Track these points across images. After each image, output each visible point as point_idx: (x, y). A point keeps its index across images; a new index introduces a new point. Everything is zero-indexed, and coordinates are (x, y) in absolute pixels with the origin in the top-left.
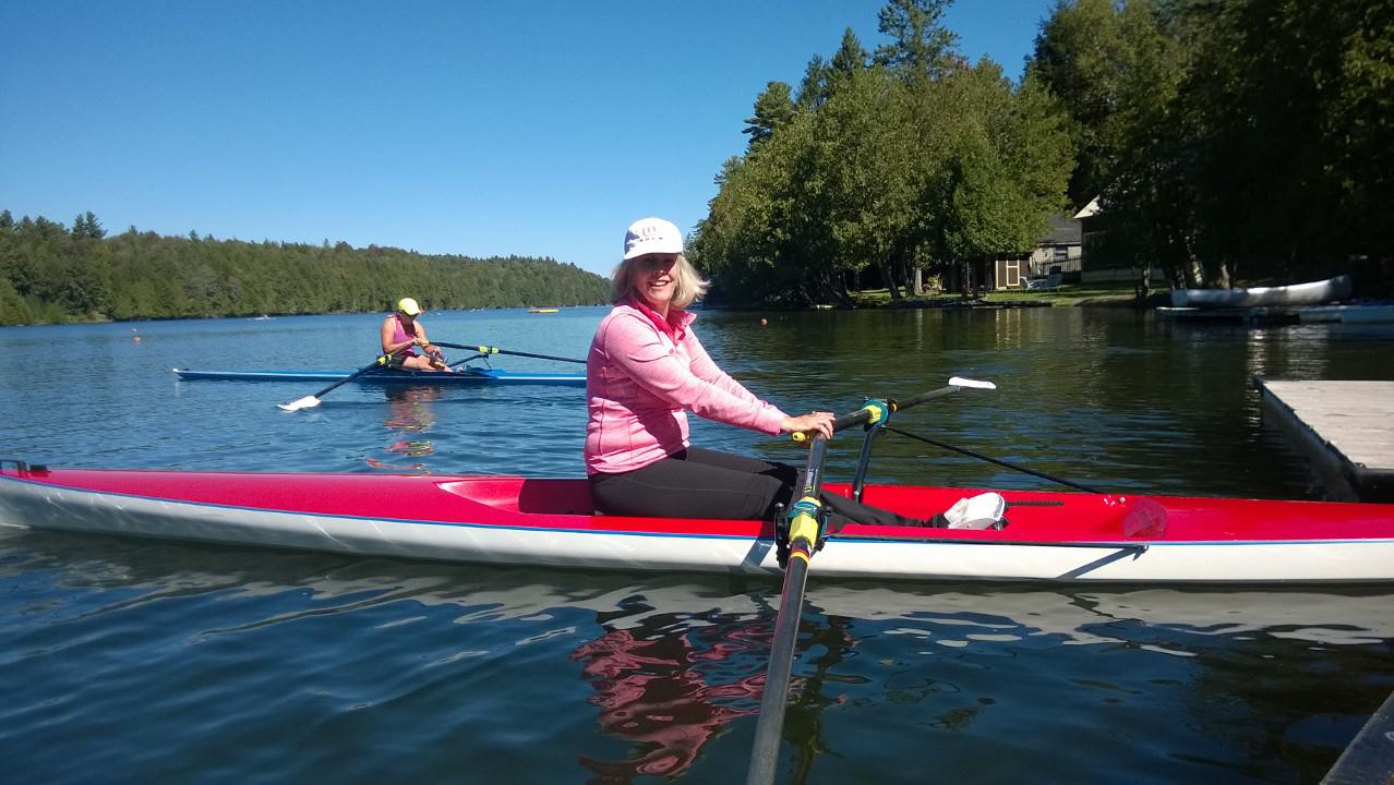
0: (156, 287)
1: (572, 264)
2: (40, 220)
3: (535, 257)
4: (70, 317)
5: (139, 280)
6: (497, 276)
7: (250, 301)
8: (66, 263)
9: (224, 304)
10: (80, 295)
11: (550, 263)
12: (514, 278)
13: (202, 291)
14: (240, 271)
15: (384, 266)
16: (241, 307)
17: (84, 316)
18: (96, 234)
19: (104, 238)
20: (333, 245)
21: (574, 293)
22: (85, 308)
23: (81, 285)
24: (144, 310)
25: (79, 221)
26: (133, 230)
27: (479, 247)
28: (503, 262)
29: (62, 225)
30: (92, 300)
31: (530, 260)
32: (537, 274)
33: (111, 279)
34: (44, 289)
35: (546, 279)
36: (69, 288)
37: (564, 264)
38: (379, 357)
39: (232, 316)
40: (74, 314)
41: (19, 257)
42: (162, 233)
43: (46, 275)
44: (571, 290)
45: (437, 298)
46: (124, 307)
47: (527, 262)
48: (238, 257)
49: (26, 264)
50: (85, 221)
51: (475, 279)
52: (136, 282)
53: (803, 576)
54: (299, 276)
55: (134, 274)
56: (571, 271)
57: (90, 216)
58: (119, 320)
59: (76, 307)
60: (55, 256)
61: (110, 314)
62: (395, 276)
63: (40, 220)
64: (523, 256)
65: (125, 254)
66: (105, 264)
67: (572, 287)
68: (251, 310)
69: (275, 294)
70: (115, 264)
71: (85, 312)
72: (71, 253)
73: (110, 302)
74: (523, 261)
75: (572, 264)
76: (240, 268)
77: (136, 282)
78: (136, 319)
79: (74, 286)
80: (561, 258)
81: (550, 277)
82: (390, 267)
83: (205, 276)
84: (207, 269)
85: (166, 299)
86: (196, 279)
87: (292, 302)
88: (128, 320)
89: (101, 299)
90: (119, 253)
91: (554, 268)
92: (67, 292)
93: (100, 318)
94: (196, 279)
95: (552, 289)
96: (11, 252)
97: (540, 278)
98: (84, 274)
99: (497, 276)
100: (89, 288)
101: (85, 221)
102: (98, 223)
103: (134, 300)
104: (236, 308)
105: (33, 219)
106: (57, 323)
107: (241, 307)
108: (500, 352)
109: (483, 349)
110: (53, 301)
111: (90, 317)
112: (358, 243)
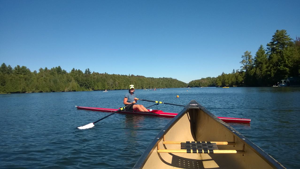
0: (102, 83)
1: (176, 79)
2: (79, 70)
3: (168, 77)
4: (85, 90)
5: (99, 82)
6: (161, 82)
7: (119, 87)
8: (85, 78)
9: (114, 87)
10: (88, 85)
11: (171, 79)
12: (164, 82)
13: (110, 84)
14: (117, 80)
15: (141, 79)
16: (118, 88)
17: (88, 89)
18: (89, 73)
19: (91, 73)
20: (131, 75)
21: (176, 85)
22: (88, 88)
23: (88, 83)
24: (100, 89)
25: (86, 70)
26: (18, 66)
27: (157, 75)
28: (162, 79)
29: (152, 77)
30: (90, 86)
31: (167, 78)
32: (169, 81)
33: (93, 82)
34: (81, 84)
35: (170, 82)
36: (86, 83)
37: (174, 79)
38: (121, 108)
39: (116, 90)
40: (86, 89)
41: (76, 77)
42: (100, 73)
43: (81, 81)
44: (176, 84)
45: (151, 86)
46: (96, 88)
47: (167, 79)
48: (116, 77)
49: (78, 79)
50: (87, 70)
51: (157, 82)
52: (98, 83)
53: (257, 145)
54: (128, 81)
55: (98, 81)
56: (175, 80)
57: (88, 69)
58: (95, 90)
59: (87, 88)
60: (83, 77)
61: (93, 89)
62: (144, 81)
63: (79, 70)
64: (101, 73)
65: (96, 77)
66: (92, 79)
67: (176, 84)
68: (119, 88)
69: (124, 85)
70: (94, 79)
71: (88, 89)
72: (86, 76)
73: (93, 87)
74: (166, 78)
75: (176, 79)
76: (117, 80)
77: (98, 83)
78: (98, 90)
79: (87, 83)
80: (173, 78)
81: (172, 82)
82: (142, 79)
83: (111, 81)
84: (111, 80)
85: (104, 86)
86: (109, 82)
87: (126, 87)
88: (96, 90)
89: (91, 86)
90: (95, 76)
91: (172, 80)
92: (85, 84)
93: (91, 90)
94: (109, 82)
95: (172, 84)
96: (75, 76)
97: (169, 82)
98: (89, 81)
99: (161, 82)
100: (89, 84)
101: (87, 70)
102: (90, 70)
103: (98, 86)
104: (116, 88)
105: (78, 70)
106: (83, 91)
107: (118, 88)
108: (164, 103)
109: (157, 102)
110: (82, 86)
111: (89, 90)
112: (136, 75)
